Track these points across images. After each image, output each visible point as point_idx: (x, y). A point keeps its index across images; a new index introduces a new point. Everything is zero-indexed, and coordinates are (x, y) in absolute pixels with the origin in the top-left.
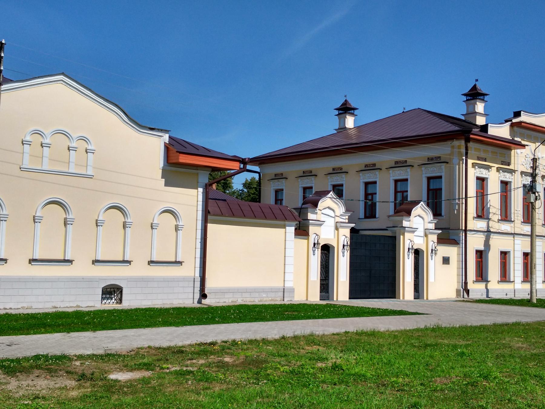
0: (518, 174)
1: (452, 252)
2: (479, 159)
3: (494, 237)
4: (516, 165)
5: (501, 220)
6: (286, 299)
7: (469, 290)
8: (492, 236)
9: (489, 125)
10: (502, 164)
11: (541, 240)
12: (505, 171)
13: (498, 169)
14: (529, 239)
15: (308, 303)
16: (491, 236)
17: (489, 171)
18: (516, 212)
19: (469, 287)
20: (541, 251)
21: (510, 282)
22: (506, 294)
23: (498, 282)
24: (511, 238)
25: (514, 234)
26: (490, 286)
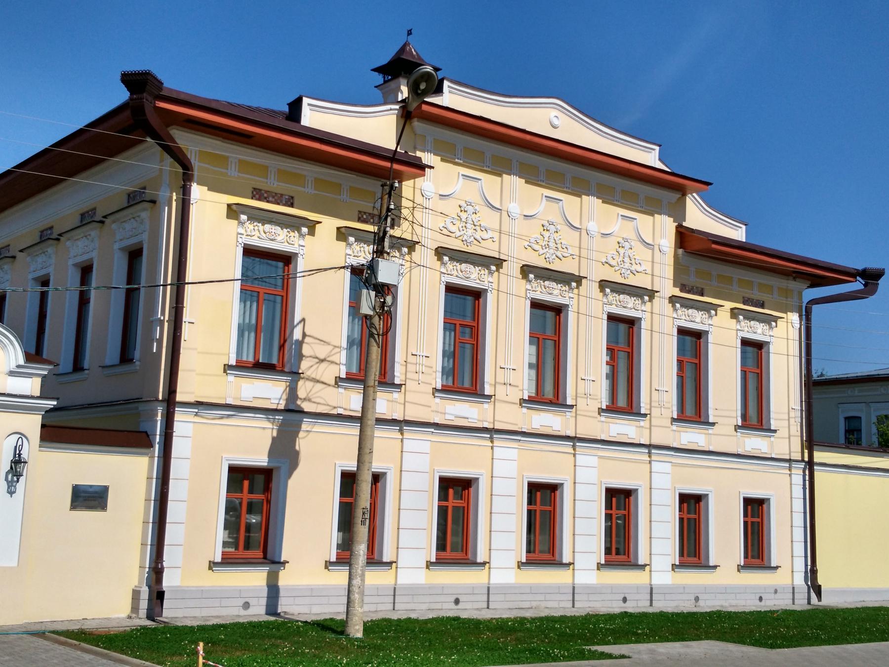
0: (590, 288)
1: (125, 473)
2: (258, 194)
3: (317, 428)
4: (656, 279)
5: (445, 390)
6: (577, 605)
7: (820, 586)
8: (354, 430)
9: (306, 101)
10: (360, 220)
11: (515, 445)
12: (750, 316)
13: (734, 313)
14: (354, 430)
15: (395, 617)
16: (304, 427)
17: (771, 328)
18: (411, 359)
19: (820, 581)
20: (669, 486)
21: (561, 564)
22: (457, 601)
23: (740, 568)
24: (567, 447)
25: (491, 432)
26: (285, 579)
